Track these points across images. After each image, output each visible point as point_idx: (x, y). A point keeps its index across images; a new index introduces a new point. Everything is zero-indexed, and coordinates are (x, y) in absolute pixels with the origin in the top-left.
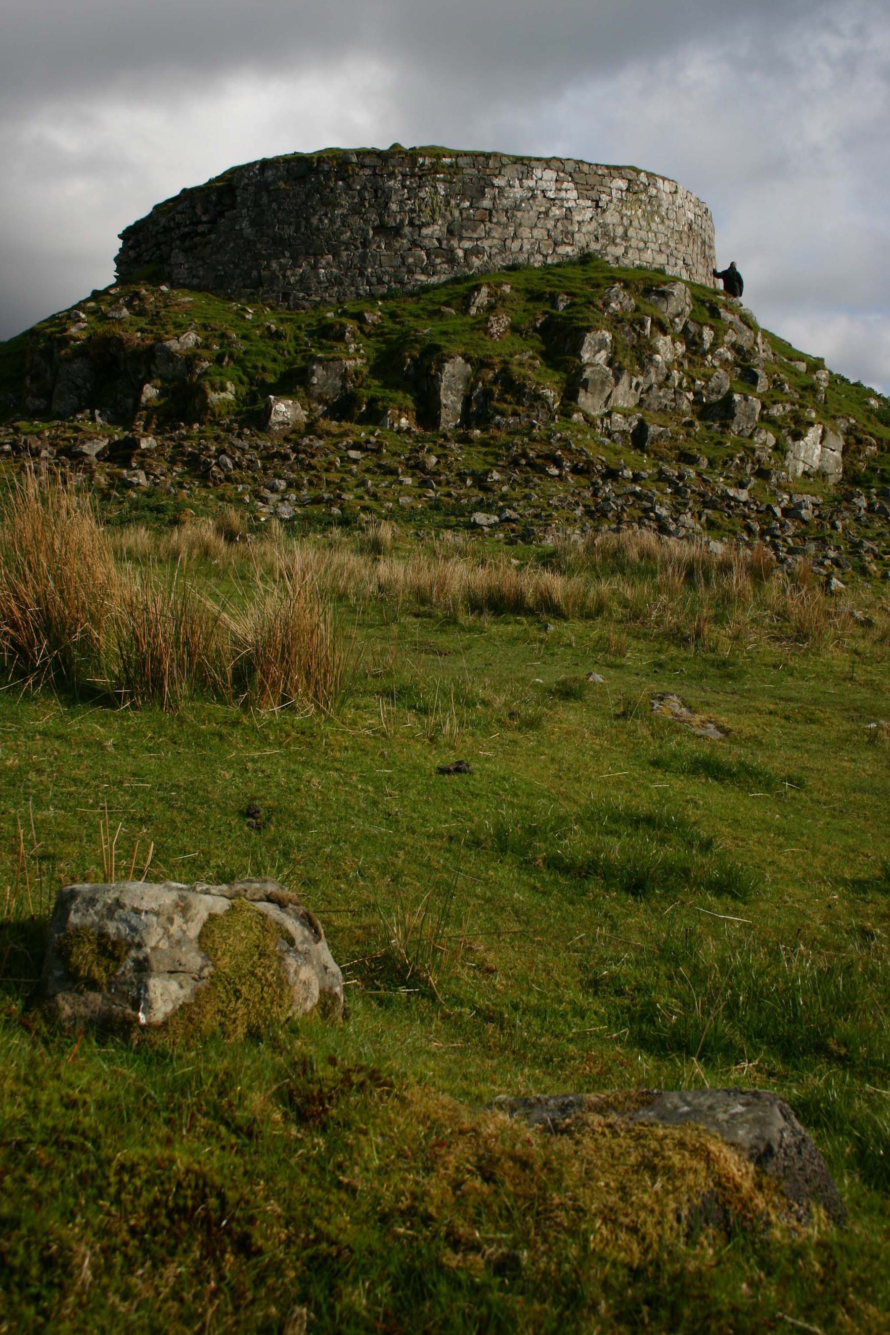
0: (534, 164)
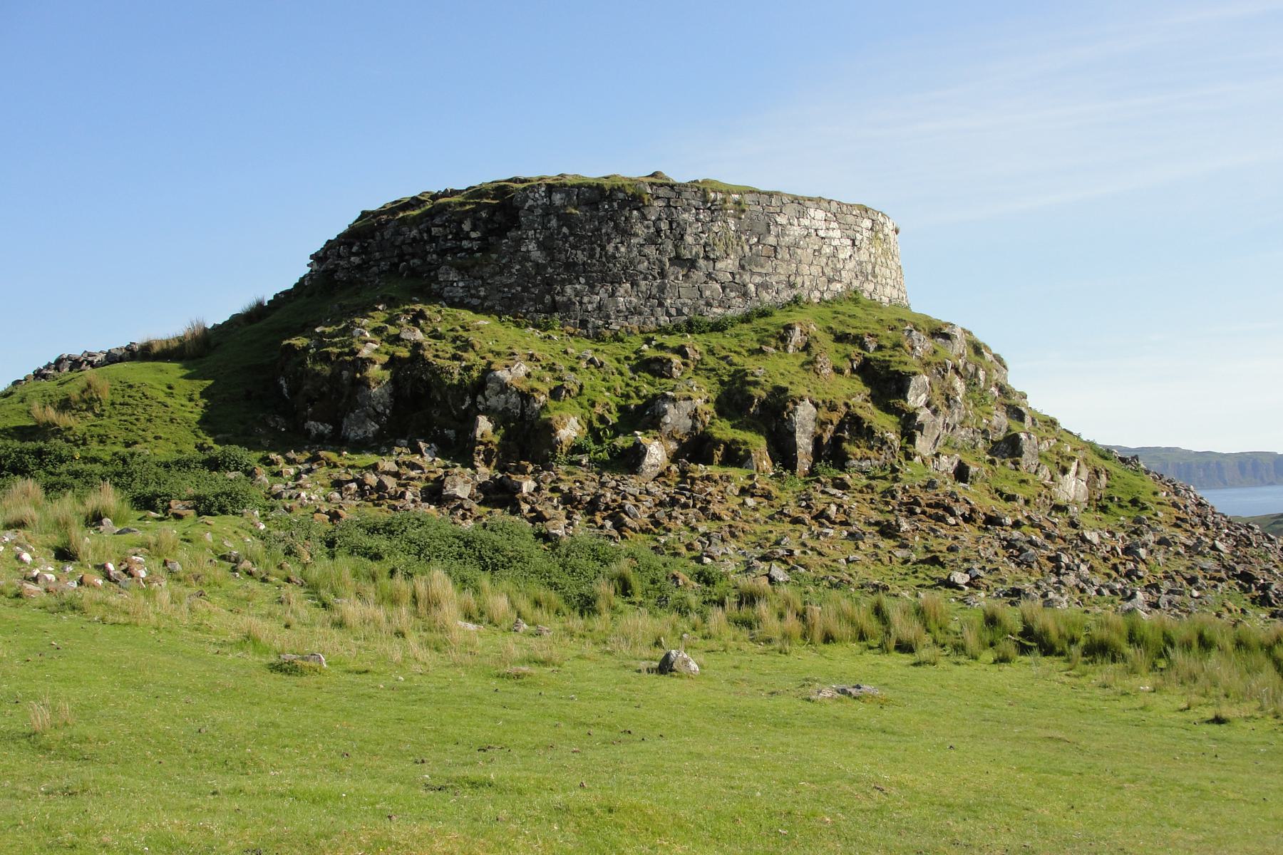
0: (808, 203)
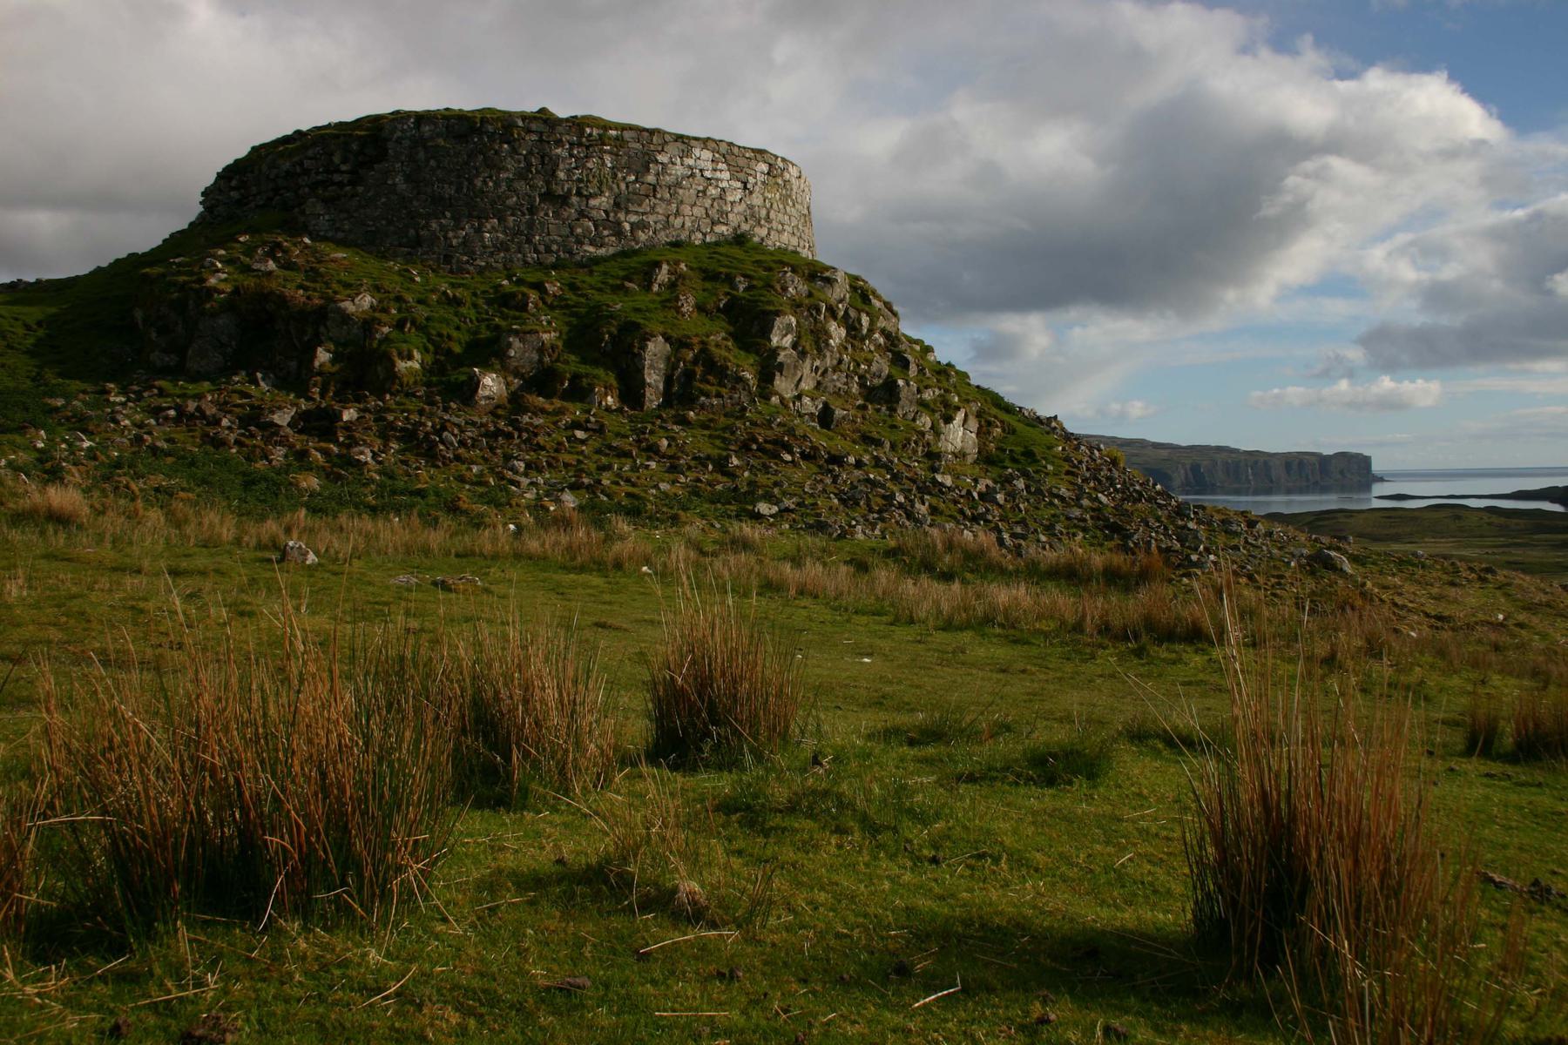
0: (693, 143)
